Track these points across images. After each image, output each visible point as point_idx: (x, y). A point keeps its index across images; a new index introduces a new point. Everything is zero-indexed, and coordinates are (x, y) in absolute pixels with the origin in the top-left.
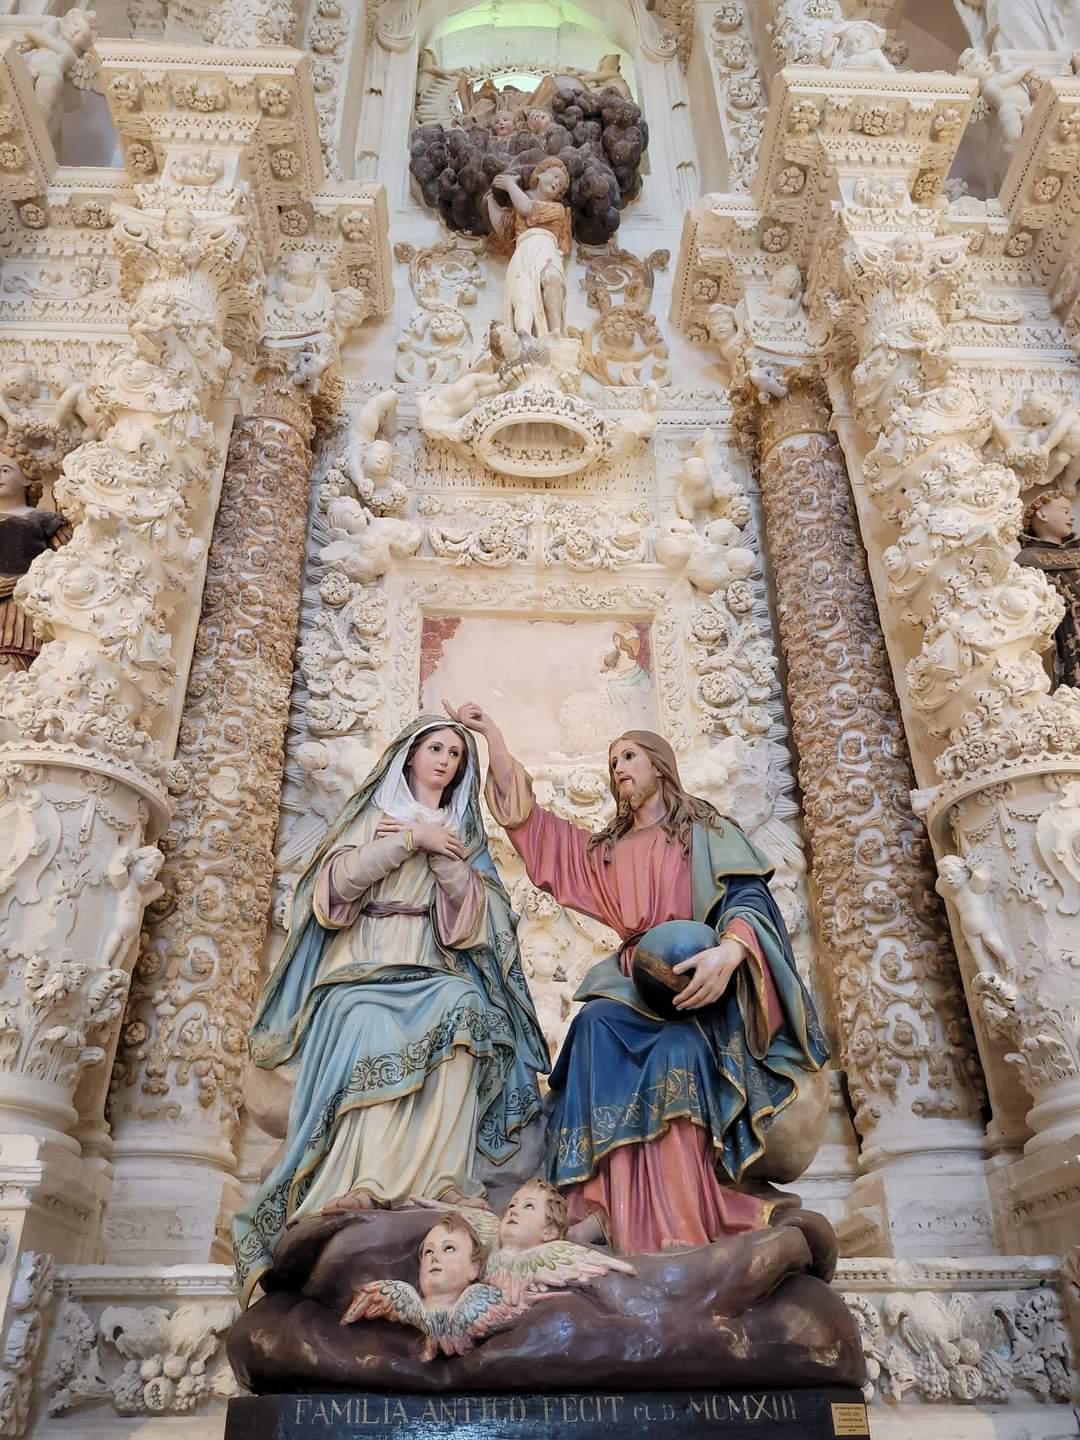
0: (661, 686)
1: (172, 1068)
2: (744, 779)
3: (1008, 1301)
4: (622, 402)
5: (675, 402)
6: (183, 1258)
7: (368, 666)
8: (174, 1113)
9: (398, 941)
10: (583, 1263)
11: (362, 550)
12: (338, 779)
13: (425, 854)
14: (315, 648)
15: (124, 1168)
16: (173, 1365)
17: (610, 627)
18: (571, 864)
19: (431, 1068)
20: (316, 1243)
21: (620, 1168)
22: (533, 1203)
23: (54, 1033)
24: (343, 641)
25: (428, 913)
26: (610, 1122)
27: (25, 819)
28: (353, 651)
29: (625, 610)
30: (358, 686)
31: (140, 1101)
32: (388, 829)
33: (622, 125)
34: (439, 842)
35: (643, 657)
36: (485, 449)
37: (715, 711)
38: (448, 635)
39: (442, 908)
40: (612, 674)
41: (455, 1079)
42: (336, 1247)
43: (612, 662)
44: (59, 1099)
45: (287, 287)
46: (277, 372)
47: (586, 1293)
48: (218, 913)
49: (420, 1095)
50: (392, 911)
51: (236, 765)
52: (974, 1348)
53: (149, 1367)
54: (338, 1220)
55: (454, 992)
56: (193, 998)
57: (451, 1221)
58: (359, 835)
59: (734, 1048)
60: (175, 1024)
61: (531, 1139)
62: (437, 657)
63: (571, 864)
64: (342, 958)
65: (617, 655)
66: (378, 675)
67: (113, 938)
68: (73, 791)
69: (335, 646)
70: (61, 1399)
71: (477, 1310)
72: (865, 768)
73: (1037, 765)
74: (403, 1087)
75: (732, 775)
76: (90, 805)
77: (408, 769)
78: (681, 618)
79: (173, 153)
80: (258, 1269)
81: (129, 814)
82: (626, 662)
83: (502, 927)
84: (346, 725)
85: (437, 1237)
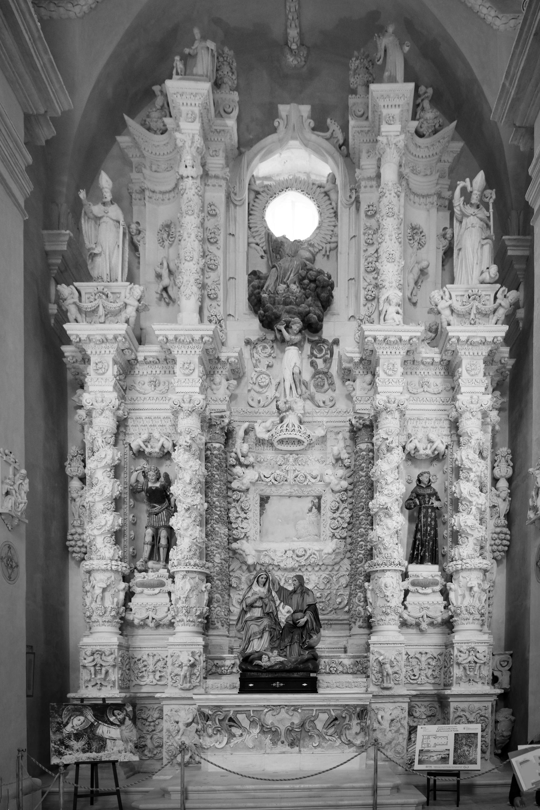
0: (322, 519)
1: (216, 620)
2: (337, 551)
3: (358, 660)
4: (318, 414)
5: (335, 414)
6: (224, 653)
7: (246, 518)
8: (217, 628)
9: (257, 612)
10: (281, 659)
11: (243, 484)
12: (241, 552)
13: (261, 598)
14: (233, 514)
15: (211, 638)
16: (226, 668)
17: (310, 499)
18: (285, 596)
19: (263, 633)
20: (249, 656)
21: (288, 647)
22: (276, 652)
23: (200, 620)
24: (240, 512)
25: (262, 607)
26: (287, 640)
27: (187, 582)
28: (243, 515)
29: (314, 494)
30: (244, 525)
31: (211, 626)
32: (254, 593)
33: (324, 287)
34: (263, 596)
35: (319, 508)
36: (275, 443)
37: (333, 531)
38: (267, 502)
39: (264, 606)
40: (310, 514)
41: (266, 635)
42: (252, 657)
43: (310, 510)
44: (201, 630)
45: (214, 387)
46: (215, 425)
47: (281, 663)
48: (220, 589)
49: (261, 637)
50: (256, 607)
51: (219, 553)
52: (352, 666)
53: (223, 668)
54: (251, 654)
55: (266, 622)
56: (218, 606)
57: (266, 654)
58: (250, 594)
59: (305, 632)
60: (215, 612)
61: (278, 642)
62: (264, 509)
63: (285, 596)
64: (248, 615)
65: (312, 508)
66: (249, 521)
67: (205, 601)
68: (194, 575)
69: (237, 513)
70: (210, 673)
71: (268, 664)
72: (363, 552)
73: (382, 568)
74: (259, 636)
75: (334, 551)
76: (197, 577)
77: (258, 581)
78: (329, 501)
79: (180, 360)
80: (241, 659)
81: (203, 577)
82: (314, 510)
83: (274, 609)
84: (242, 537)
85: (264, 656)
